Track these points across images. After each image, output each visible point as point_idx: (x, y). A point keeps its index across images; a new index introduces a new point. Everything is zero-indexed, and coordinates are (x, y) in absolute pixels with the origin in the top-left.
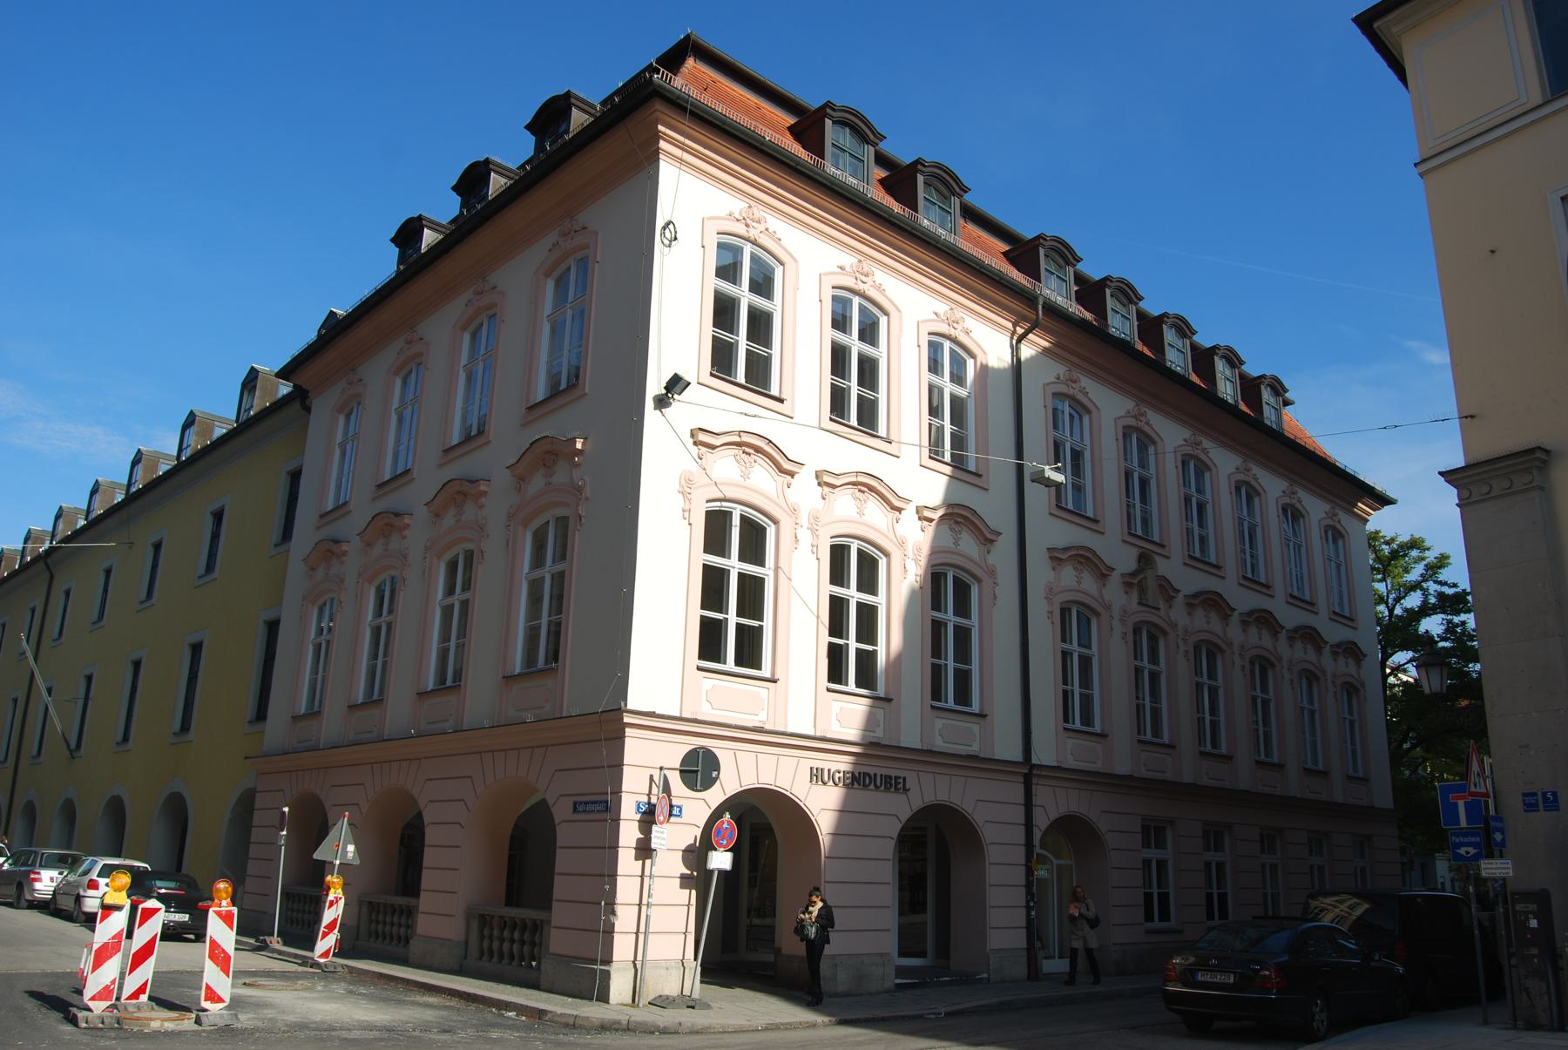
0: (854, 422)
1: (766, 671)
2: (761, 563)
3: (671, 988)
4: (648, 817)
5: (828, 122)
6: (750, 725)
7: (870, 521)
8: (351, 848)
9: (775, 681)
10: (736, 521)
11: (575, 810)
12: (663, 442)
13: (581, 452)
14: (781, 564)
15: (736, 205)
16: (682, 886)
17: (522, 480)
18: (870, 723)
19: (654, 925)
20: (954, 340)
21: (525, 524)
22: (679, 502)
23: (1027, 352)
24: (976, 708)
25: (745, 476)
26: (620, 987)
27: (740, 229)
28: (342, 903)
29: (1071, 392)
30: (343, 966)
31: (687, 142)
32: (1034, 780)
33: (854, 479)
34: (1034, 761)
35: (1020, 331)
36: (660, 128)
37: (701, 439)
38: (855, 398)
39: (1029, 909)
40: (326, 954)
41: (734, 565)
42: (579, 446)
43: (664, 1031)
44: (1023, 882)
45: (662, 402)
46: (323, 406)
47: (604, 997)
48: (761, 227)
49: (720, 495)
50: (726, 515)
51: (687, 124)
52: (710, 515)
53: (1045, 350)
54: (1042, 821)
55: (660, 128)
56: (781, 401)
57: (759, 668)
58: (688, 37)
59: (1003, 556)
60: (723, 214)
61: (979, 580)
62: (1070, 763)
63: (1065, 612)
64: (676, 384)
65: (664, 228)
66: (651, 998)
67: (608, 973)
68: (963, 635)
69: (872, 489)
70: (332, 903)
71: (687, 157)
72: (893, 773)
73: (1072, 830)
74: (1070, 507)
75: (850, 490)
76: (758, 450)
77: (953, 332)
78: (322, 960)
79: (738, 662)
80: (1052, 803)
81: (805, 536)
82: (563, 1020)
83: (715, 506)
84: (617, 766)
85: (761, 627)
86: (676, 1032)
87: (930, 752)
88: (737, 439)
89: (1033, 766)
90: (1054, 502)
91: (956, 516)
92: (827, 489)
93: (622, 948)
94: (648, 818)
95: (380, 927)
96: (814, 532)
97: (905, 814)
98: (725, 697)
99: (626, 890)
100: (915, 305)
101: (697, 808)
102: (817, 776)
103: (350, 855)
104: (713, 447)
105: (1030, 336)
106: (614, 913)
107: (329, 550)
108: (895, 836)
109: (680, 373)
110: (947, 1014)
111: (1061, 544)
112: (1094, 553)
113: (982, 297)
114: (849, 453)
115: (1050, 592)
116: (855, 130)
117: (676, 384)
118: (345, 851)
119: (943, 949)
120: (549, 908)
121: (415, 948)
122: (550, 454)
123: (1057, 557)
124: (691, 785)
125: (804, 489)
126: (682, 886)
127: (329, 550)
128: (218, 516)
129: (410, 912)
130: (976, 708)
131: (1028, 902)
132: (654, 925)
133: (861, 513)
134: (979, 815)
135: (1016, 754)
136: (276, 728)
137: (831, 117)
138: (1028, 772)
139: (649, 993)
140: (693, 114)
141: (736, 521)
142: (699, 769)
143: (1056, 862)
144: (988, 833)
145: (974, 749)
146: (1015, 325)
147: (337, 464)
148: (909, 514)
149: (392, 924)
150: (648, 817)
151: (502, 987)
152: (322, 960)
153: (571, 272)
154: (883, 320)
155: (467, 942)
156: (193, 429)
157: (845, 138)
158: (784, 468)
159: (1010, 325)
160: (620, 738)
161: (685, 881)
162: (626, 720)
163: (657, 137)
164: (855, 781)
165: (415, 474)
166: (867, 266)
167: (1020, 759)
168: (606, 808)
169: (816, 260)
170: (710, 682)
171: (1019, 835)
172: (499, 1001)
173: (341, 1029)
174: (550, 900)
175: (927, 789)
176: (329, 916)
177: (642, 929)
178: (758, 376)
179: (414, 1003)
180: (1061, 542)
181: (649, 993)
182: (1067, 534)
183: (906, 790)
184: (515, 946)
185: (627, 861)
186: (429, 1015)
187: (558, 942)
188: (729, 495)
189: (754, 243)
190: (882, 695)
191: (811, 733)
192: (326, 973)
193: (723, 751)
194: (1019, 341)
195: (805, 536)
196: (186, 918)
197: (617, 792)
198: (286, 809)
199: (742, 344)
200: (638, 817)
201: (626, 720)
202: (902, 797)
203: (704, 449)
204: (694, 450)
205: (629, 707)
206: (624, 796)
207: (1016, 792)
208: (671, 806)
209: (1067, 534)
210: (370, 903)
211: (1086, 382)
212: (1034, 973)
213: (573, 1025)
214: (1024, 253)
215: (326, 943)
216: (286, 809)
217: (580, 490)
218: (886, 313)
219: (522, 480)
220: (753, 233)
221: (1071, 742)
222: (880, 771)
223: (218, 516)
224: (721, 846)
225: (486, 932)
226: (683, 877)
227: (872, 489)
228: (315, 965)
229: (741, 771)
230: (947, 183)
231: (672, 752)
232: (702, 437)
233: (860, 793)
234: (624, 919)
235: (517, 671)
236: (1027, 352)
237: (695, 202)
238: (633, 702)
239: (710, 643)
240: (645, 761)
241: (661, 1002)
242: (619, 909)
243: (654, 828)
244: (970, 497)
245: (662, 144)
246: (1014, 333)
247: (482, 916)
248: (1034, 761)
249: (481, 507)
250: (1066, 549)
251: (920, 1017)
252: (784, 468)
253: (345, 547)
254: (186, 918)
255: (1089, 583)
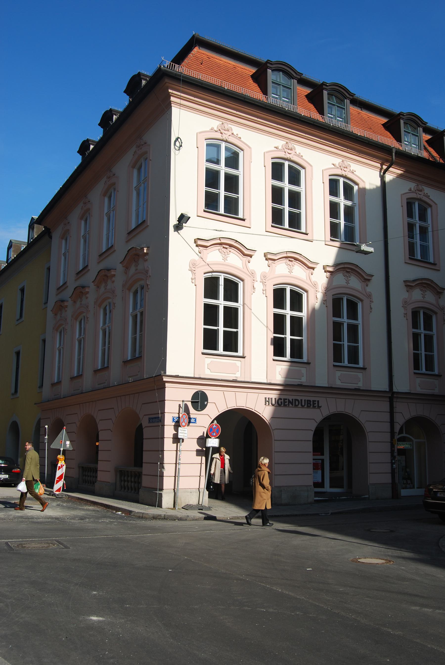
0: (287, 225)
1: (240, 353)
2: (236, 301)
3: (194, 501)
4: (177, 425)
5: (269, 71)
6: (231, 379)
7: (296, 275)
8: (68, 443)
9: (244, 357)
10: (222, 282)
11: (149, 422)
12: (180, 249)
13: (147, 254)
14: (246, 302)
15: (215, 123)
16: (197, 455)
17: (127, 268)
18: (289, 374)
19: (185, 472)
20: (345, 177)
21: (129, 289)
22: (190, 274)
23: (389, 177)
24: (361, 365)
25: (225, 259)
26: (167, 500)
27: (218, 136)
28: (64, 467)
29: (419, 196)
30: (66, 495)
31: (182, 95)
32: (395, 400)
33: (285, 255)
34: (395, 390)
35: (385, 167)
36: (170, 91)
37: (200, 243)
38: (286, 212)
39: (392, 464)
40: (59, 490)
41: (221, 303)
42: (145, 251)
43: (180, 519)
44: (389, 451)
45: (178, 228)
46: (56, 235)
47: (160, 506)
48: (230, 133)
49: (210, 270)
50: (216, 279)
51: (181, 86)
52: (207, 280)
53: (400, 176)
54: (400, 420)
55: (170, 91)
56: (243, 220)
57: (236, 351)
58: (194, 36)
59: (376, 287)
60: (208, 129)
61: (362, 300)
62: (419, 390)
63: (415, 314)
64: (183, 219)
65: (175, 142)
66: (182, 506)
67: (161, 494)
68: (353, 329)
69: (296, 259)
70: (59, 468)
71: (183, 102)
72: (312, 399)
73: (417, 424)
74: (419, 258)
75: (284, 261)
76: (231, 246)
77: (344, 173)
78: (57, 493)
79: (225, 350)
80: (405, 412)
81: (259, 286)
82: (138, 515)
83: (209, 275)
84: (162, 401)
85: (237, 332)
86: (186, 520)
87: (331, 388)
88: (219, 241)
89: (394, 393)
90: (407, 256)
91: (341, 268)
92: (270, 261)
93: (168, 483)
94: (177, 424)
95: (126, 483)
96: (264, 283)
97: (319, 418)
98: (219, 366)
99: (169, 456)
100: (319, 162)
101: (204, 419)
102: (267, 401)
103: (68, 446)
104: (206, 247)
105: (391, 169)
106: (163, 468)
107: (60, 306)
108: (314, 429)
109: (183, 213)
110: (332, 514)
111: (411, 278)
112: (432, 281)
113: (360, 152)
114: (285, 242)
115: (405, 303)
116: (286, 73)
117: (183, 219)
118: (65, 445)
119: (350, 485)
120: (141, 466)
121: (97, 486)
122: (134, 256)
123: (409, 285)
124: (196, 408)
125: (258, 264)
126: (197, 455)
127: (60, 306)
128: (22, 290)
129: (139, 475)
130: (361, 365)
131: (392, 460)
132: (185, 472)
133: (290, 272)
134: (362, 418)
135: (385, 387)
136: (47, 391)
137: (270, 68)
138: (391, 396)
139: (182, 502)
140: (183, 81)
141: (222, 282)
142: (200, 401)
143: (415, 440)
144: (368, 427)
145: (360, 385)
146: (382, 165)
147: (65, 261)
148: (319, 270)
149: (128, 481)
150: (177, 425)
151: (124, 502)
152: (57, 493)
153: (139, 164)
154: (302, 172)
155: (116, 483)
156: (12, 249)
157: (280, 78)
158: (246, 254)
159: (379, 165)
160: (163, 388)
161: (199, 453)
162: (164, 380)
163: (169, 96)
164: (280, 403)
165: (89, 267)
166: (291, 145)
167: (388, 390)
168: (158, 420)
169: (260, 145)
170: (209, 360)
171: (387, 427)
172: (117, 507)
173: (36, 518)
174: (142, 463)
175: (330, 406)
176: (59, 473)
177: (177, 475)
178: (232, 207)
179: (80, 509)
180: (411, 277)
181: (182, 502)
182: (416, 272)
183: (319, 407)
184: (129, 483)
185: (168, 444)
186: (81, 513)
187: (146, 481)
188: (215, 269)
189: (226, 141)
190: (306, 361)
191: (265, 381)
192: (58, 498)
193: (210, 393)
194: (384, 173)
195: (259, 286)
196: (7, 476)
197: (163, 413)
198: (47, 426)
199: (222, 192)
200: (174, 424)
201: (164, 380)
202: (317, 411)
203: (201, 248)
204: (197, 249)
205: (168, 373)
206: (166, 415)
207: (386, 406)
208: (190, 418)
209: (416, 272)
210: (83, 467)
211: (428, 190)
212: (395, 495)
213: (142, 517)
214: (393, 123)
215: (58, 485)
216: (47, 426)
217: (147, 272)
218: (304, 168)
219: (127, 268)
220: (225, 137)
221: (418, 380)
222: (304, 398)
223: (22, 290)
224: (213, 436)
225: (122, 478)
226: (197, 451)
227: (296, 259)
228: (54, 495)
229: (220, 401)
230: (341, 94)
231: (186, 394)
232: (199, 242)
233: (282, 409)
234: (168, 470)
235: (129, 358)
236: (389, 177)
237: (191, 127)
238: (170, 370)
239: (210, 341)
240: (175, 397)
241: (187, 507)
242: (165, 466)
243: (180, 428)
244: (352, 258)
245: (172, 99)
246: (381, 169)
247: (121, 471)
248: (395, 390)
249: (113, 282)
250: (414, 281)
251: (317, 514)
252: (246, 254)
253: (66, 304)
254: (7, 476)
255: (430, 297)
